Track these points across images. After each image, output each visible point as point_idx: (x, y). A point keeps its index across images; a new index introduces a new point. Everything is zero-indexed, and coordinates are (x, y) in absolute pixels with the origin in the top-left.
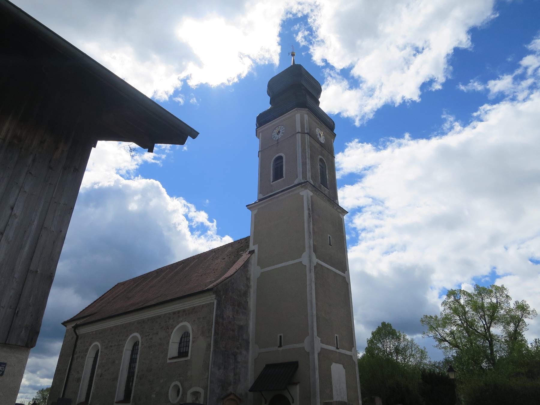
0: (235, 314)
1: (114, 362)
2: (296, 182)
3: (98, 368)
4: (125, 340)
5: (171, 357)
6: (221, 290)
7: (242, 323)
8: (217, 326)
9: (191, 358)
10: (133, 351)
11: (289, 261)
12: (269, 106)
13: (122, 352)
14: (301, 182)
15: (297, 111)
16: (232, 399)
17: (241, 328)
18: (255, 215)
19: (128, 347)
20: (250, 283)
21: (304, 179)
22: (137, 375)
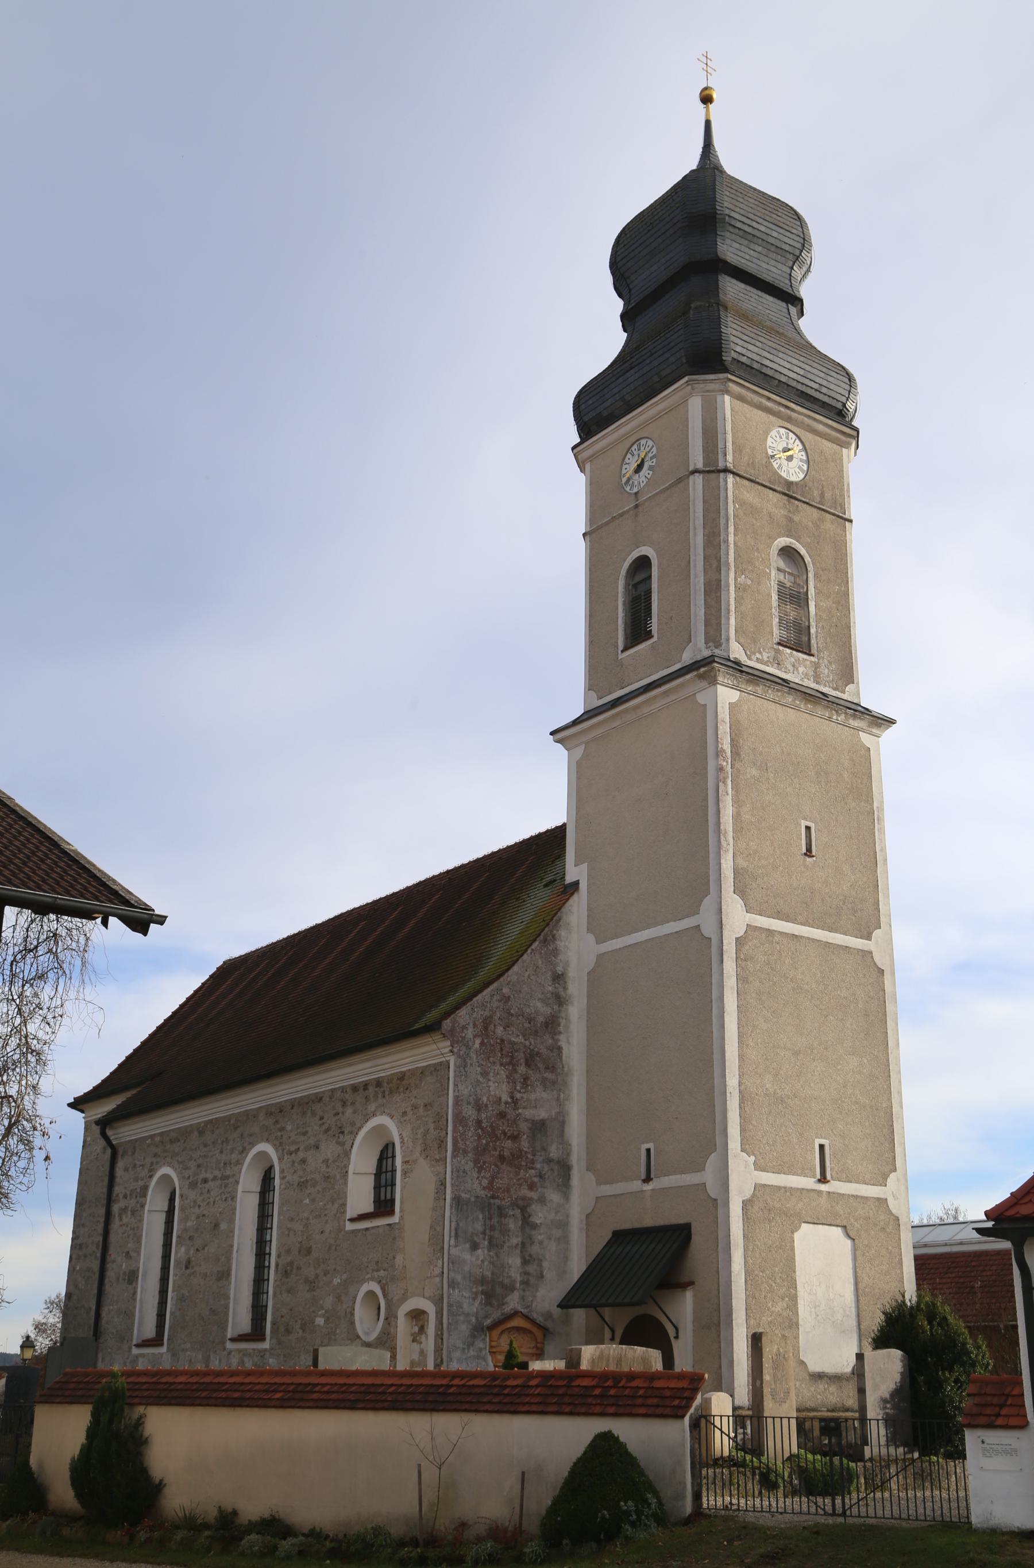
0: (518, 1088)
1: (216, 1226)
2: (687, 657)
3: (177, 1241)
4: (239, 1163)
5: (355, 1215)
6: (468, 1024)
7: (542, 1114)
8: (461, 1128)
9: (401, 1218)
10: (378, 1175)
11: (668, 922)
12: (626, 334)
13: (233, 1198)
14: (699, 658)
15: (690, 387)
16: (518, 1329)
17: (539, 1127)
18: (579, 764)
19: (248, 1183)
20: (565, 989)
21: (711, 644)
22: (277, 1265)
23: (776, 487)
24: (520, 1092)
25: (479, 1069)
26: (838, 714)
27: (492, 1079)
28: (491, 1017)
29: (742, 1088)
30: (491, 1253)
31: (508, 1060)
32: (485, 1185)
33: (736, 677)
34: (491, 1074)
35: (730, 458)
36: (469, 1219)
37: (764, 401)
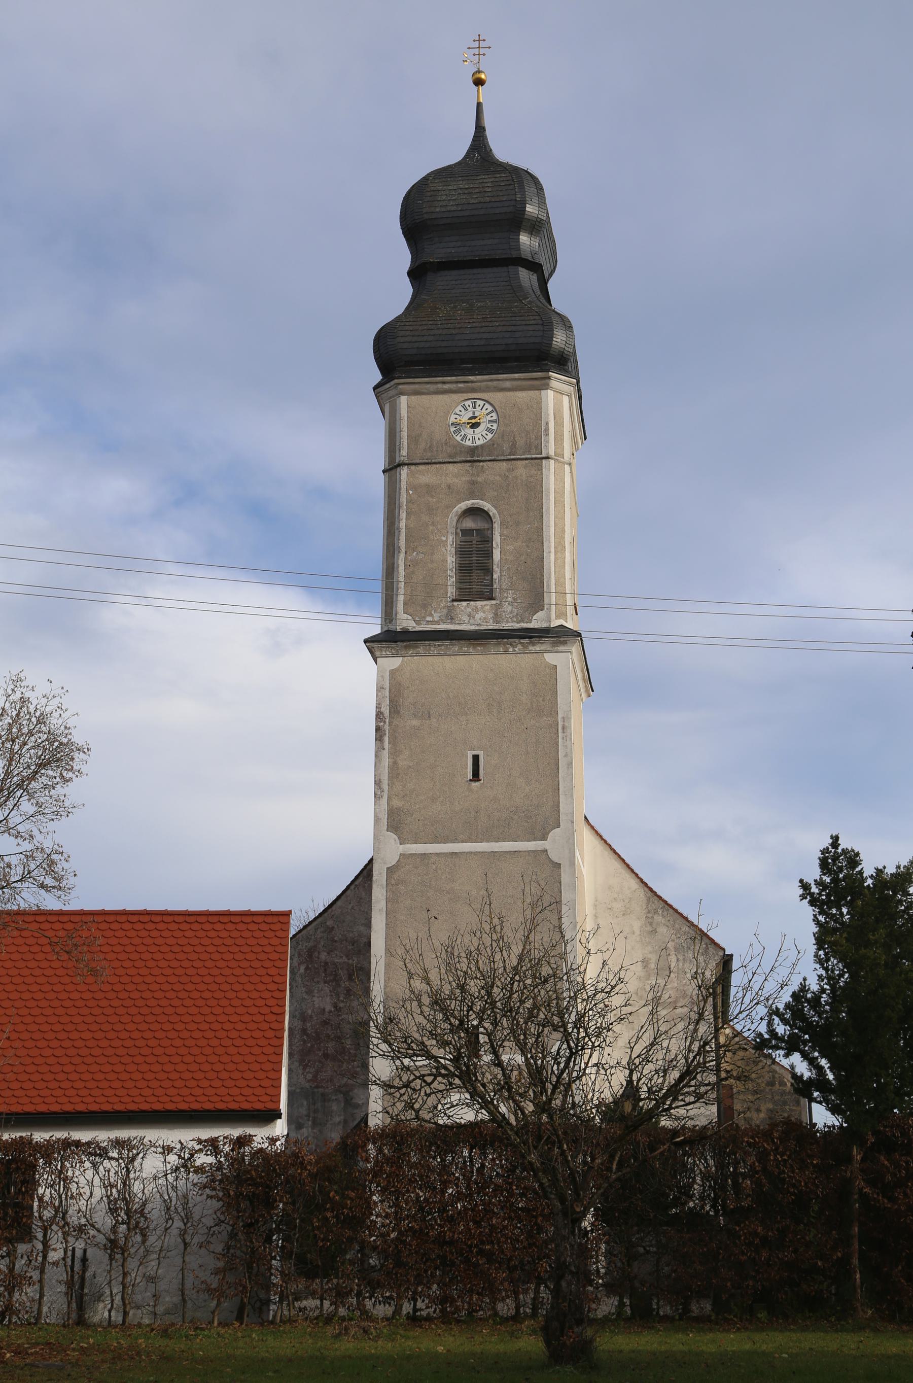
23: (455, 460)
24: (343, 1001)
25: (304, 989)
26: (514, 647)
27: (317, 995)
28: (315, 946)
29: (388, 989)
30: (315, 1131)
31: (332, 978)
32: (309, 1078)
33: (392, 648)
34: (316, 991)
35: (404, 452)
36: (295, 1106)
37: (440, 386)
